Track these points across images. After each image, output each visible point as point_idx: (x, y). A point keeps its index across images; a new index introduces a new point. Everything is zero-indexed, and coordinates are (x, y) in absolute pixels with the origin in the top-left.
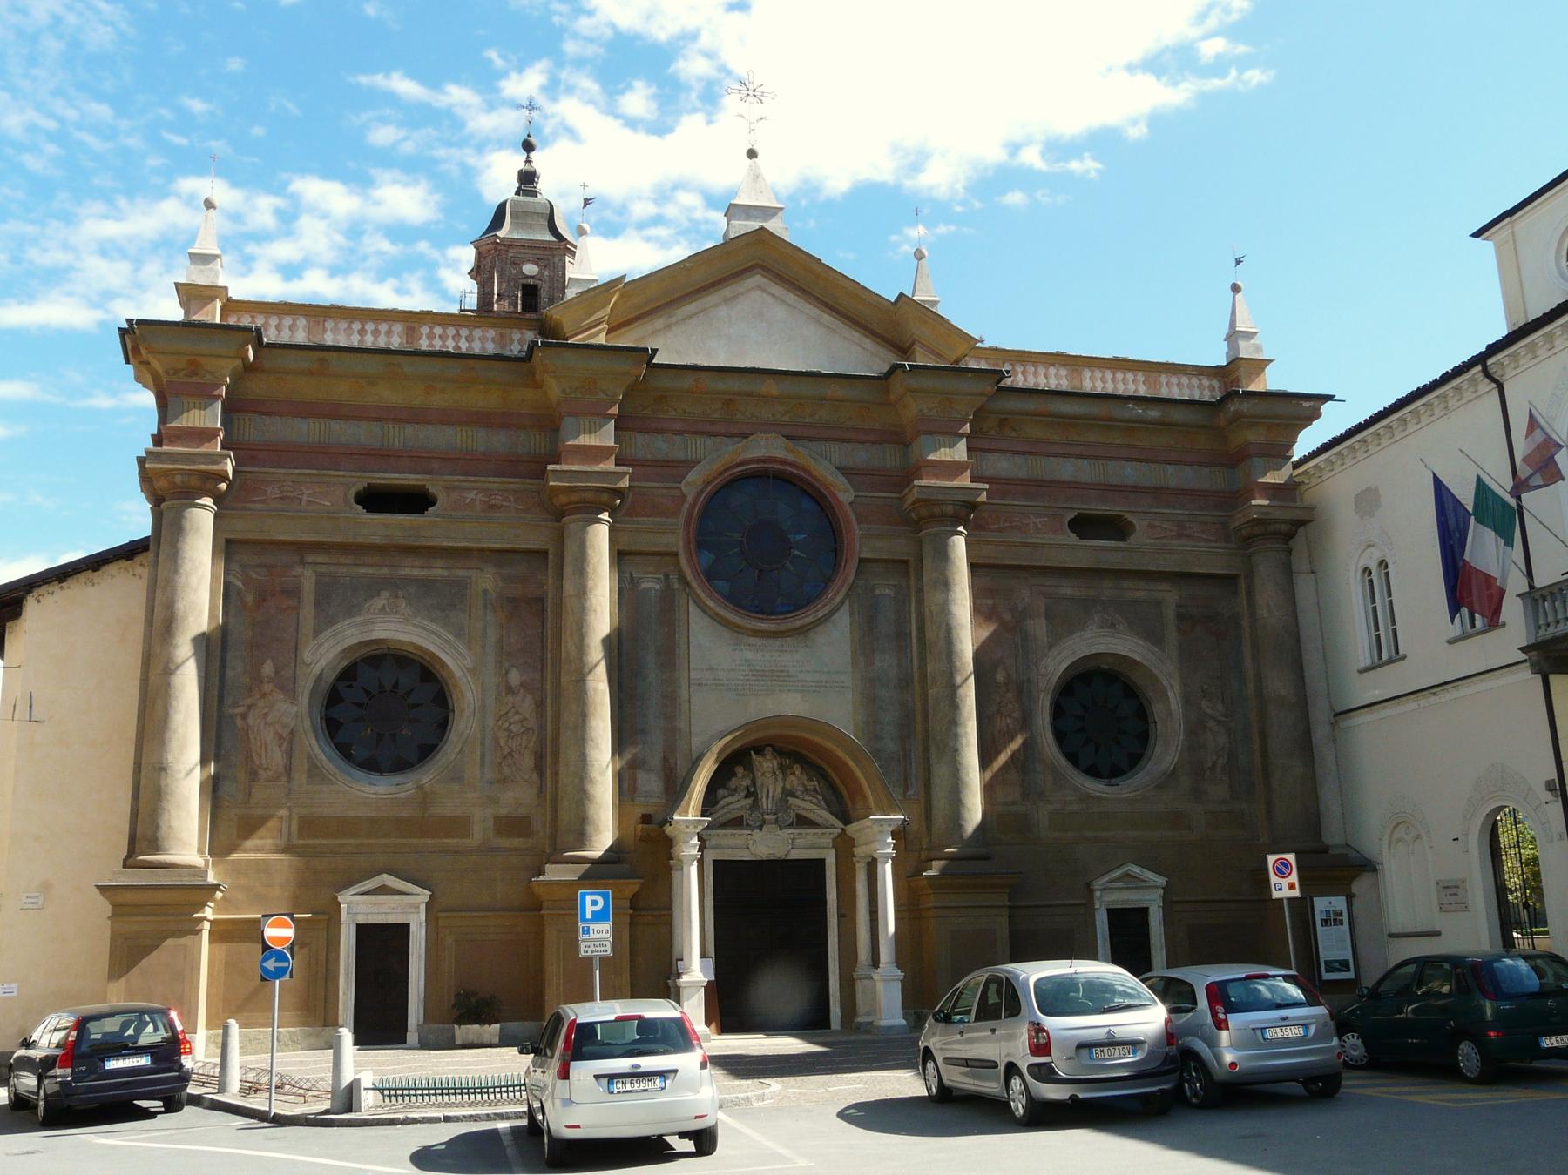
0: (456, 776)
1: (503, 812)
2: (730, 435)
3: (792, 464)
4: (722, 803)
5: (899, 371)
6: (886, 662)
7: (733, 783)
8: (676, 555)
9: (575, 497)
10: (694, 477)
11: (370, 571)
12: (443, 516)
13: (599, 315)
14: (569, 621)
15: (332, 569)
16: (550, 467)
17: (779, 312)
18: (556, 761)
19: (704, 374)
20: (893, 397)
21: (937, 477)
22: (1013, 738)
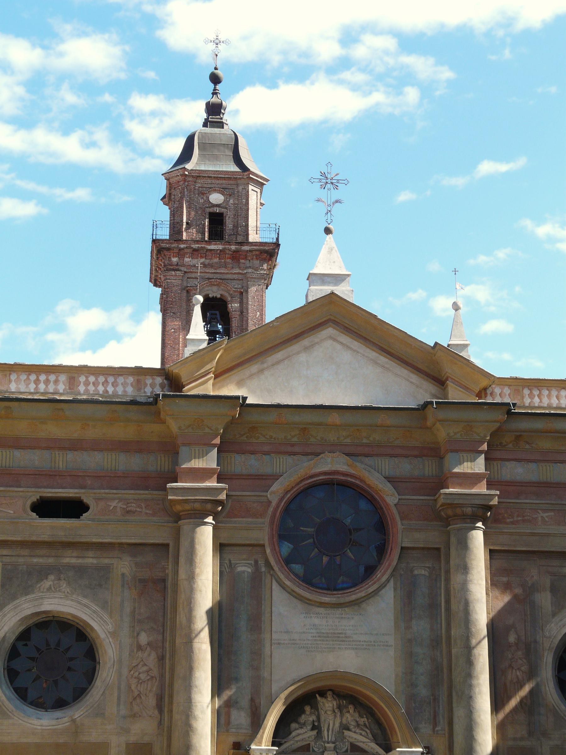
0: (99, 712)
1: (132, 739)
2: (306, 454)
3: (352, 476)
4: (294, 734)
5: (429, 406)
6: (421, 627)
7: (303, 718)
8: (263, 546)
9: (188, 507)
10: (277, 487)
11: (41, 560)
12: (93, 520)
13: (208, 367)
14: (182, 598)
15: (13, 559)
16: (169, 485)
17: (346, 356)
18: (171, 703)
19: (286, 410)
20: (429, 423)
21: (461, 485)
22: (521, 687)
